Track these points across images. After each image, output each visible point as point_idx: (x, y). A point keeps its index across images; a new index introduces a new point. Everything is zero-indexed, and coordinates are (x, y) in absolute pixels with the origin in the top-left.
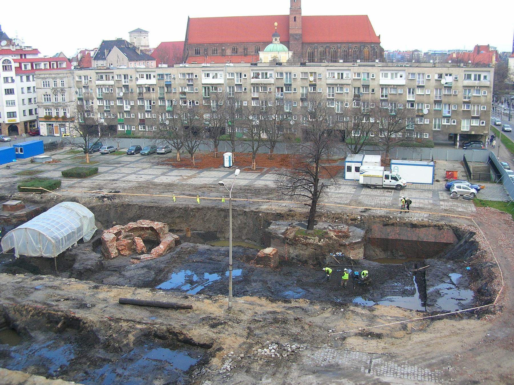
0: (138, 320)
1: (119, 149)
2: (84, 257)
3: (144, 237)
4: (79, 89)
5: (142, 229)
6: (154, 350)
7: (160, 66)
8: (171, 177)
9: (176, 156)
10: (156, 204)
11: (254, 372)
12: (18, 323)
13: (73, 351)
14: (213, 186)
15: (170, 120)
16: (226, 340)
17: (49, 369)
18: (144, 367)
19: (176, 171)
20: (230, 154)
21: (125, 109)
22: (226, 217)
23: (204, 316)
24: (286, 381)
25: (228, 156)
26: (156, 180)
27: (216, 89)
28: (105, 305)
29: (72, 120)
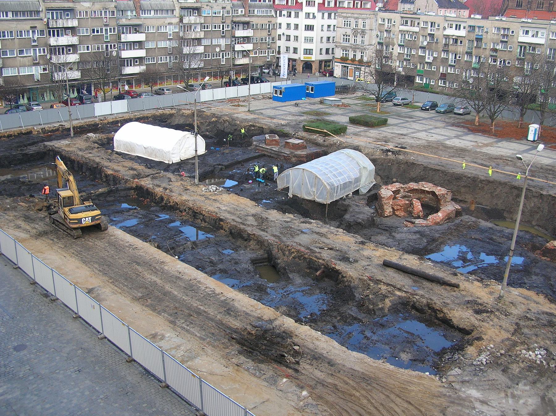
0: (399, 286)
1: (414, 103)
2: (357, 210)
3: (423, 201)
4: (381, 32)
5: (423, 192)
6: (408, 321)
7: (472, 16)
8: (465, 142)
9: (475, 119)
10: (443, 168)
11: (512, 373)
12: (279, 261)
13: (326, 302)
14: (510, 159)
15: (475, 78)
16: (489, 331)
17: (300, 314)
18: (394, 336)
19: (472, 135)
20: (536, 126)
21: (427, 60)
22: (519, 196)
23: (470, 299)
24: (547, 394)
25: (533, 129)
26: (448, 142)
27: (534, 49)
28: (368, 263)
29: (368, 64)
